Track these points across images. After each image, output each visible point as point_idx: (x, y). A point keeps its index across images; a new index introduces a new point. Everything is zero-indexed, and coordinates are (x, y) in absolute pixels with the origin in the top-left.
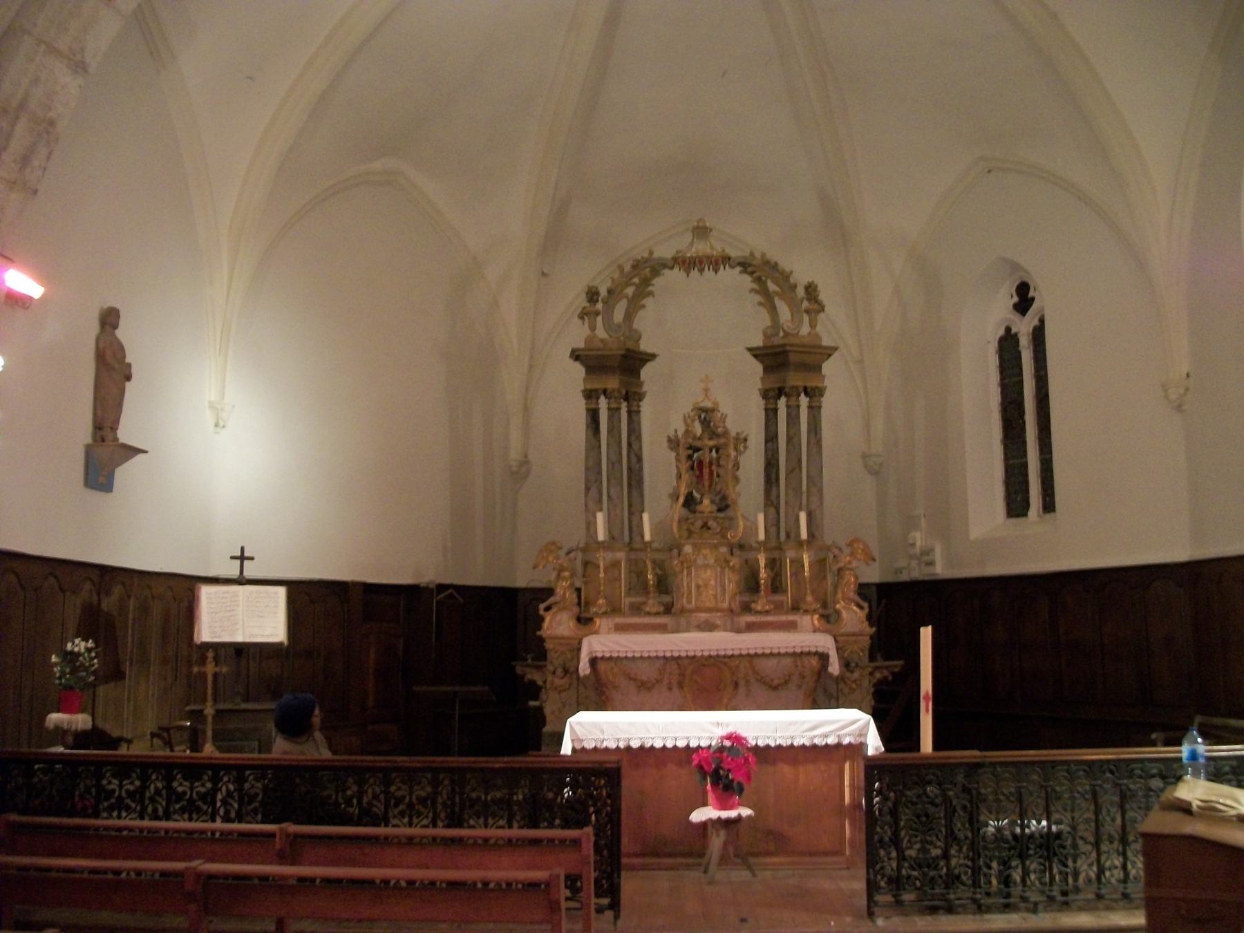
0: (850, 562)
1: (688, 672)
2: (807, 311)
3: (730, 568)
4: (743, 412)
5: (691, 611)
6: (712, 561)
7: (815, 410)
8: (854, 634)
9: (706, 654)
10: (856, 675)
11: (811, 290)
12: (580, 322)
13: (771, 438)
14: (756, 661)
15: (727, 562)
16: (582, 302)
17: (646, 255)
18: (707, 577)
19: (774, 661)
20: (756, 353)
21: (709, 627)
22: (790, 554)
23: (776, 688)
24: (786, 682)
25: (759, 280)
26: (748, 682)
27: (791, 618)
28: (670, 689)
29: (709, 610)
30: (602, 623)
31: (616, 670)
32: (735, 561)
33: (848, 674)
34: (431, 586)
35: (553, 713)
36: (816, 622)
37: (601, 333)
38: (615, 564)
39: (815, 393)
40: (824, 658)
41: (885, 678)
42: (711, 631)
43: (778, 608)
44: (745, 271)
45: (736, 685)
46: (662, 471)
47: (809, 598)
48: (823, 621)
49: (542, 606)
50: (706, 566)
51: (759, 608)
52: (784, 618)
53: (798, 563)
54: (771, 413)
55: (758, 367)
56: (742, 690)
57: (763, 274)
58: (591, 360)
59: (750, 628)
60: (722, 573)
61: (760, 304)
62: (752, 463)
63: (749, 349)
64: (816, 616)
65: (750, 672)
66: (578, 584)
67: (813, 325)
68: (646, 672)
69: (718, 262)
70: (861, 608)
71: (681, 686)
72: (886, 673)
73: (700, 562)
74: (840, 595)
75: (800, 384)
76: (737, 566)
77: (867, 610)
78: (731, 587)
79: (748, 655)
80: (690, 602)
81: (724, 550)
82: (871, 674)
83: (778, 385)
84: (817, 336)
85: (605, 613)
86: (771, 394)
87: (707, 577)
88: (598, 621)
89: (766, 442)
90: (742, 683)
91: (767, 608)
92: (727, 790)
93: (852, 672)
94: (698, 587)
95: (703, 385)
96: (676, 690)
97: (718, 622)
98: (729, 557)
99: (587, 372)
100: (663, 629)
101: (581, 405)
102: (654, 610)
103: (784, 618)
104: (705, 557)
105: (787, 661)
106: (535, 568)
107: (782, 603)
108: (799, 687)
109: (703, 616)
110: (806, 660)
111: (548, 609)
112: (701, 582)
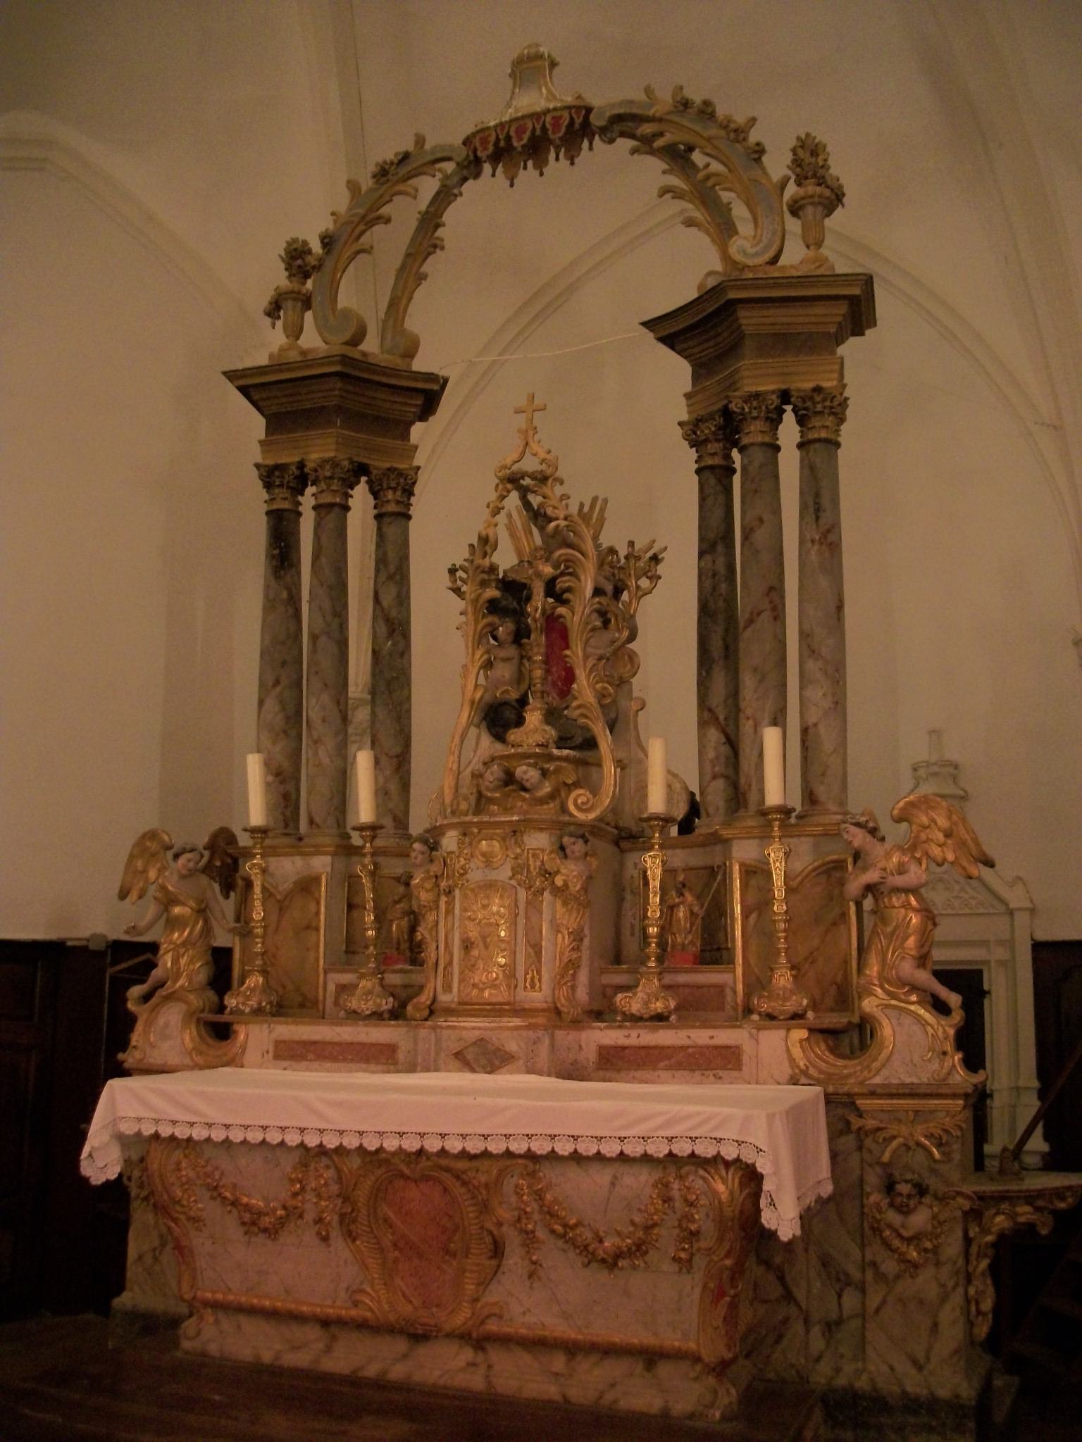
0: (901, 870)
1: (361, 1195)
2: (795, 210)
3: (558, 891)
4: (645, 489)
5: (449, 1012)
6: (504, 874)
7: (820, 448)
8: (912, 1093)
9: (412, 1145)
10: (920, 1219)
11: (809, 158)
12: (268, 320)
13: (714, 541)
14: (548, 1173)
15: (548, 874)
16: (280, 278)
17: (408, 145)
18: (502, 921)
19: (601, 1177)
20: (676, 330)
21: (488, 1058)
22: (743, 851)
23: (611, 1262)
24: (640, 1249)
25: (678, 156)
26: (529, 1240)
27: (724, 1037)
28: (325, 1239)
29: (495, 1010)
30: (255, 1037)
31: (188, 1172)
32: (570, 873)
33: (893, 1217)
34: (92, 946)
35: (140, 1258)
36: (797, 1052)
37: (311, 339)
38: (307, 886)
39: (822, 411)
40: (752, 1177)
41: (1031, 1227)
42: (492, 1069)
43: (695, 1006)
44: (646, 145)
45: (497, 1250)
46: (447, 659)
47: (783, 979)
48: (821, 1049)
49: (136, 991)
50: (490, 886)
51: (636, 1007)
52: (701, 1037)
53: (757, 873)
54: (714, 476)
55: (674, 372)
56: (514, 1259)
57: (684, 140)
58: (280, 396)
59: (612, 1063)
60: (534, 904)
61: (634, 151)
62: (667, 622)
63: (649, 325)
64: (800, 1034)
65: (532, 1207)
66: (222, 940)
67: (814, 241)
68: (264, 1188)
69: (574, 130)
70: (941, 1008)
71: (351, 1236)
72: (1025, 1213)
73: (476, 875)
74: (873, 969)
75: (769, 386)
76: (576, 887)
77: (958, 1016)
78: (554, 946)
79: (530, 1156)
80: (448, 988)
81: (539, 841)
82: (974, 1215)
83: (720, 405)
84: (823, 261)
85: (258, 1011)
86: (708, 429)
87: (502, 921)
88: (241, 1032)
89: (701, 554)
90: (513, 1240)
91: (658, 1006)
92: (1063, 1199)
93: (905, 1211)
94: (467, 945)
95: (521, 420)
96: (338, 1241)
97: (512, 1046)
98: (552, 862)
99: (270, 429)
100: (385, 1057)
101: (254, 503)
102: (367, 1007)
103: (701, 1037)
104: (488, 859)
105: (639, 1182)
106: (123, 895)
107: (720, 988)
108: (685, 1265)
109: (472, 1027)
110: (696, 1181)
111: (146, 998)
112: (474, 934)
